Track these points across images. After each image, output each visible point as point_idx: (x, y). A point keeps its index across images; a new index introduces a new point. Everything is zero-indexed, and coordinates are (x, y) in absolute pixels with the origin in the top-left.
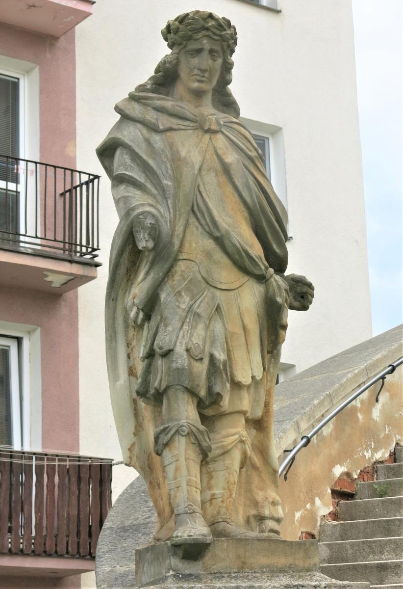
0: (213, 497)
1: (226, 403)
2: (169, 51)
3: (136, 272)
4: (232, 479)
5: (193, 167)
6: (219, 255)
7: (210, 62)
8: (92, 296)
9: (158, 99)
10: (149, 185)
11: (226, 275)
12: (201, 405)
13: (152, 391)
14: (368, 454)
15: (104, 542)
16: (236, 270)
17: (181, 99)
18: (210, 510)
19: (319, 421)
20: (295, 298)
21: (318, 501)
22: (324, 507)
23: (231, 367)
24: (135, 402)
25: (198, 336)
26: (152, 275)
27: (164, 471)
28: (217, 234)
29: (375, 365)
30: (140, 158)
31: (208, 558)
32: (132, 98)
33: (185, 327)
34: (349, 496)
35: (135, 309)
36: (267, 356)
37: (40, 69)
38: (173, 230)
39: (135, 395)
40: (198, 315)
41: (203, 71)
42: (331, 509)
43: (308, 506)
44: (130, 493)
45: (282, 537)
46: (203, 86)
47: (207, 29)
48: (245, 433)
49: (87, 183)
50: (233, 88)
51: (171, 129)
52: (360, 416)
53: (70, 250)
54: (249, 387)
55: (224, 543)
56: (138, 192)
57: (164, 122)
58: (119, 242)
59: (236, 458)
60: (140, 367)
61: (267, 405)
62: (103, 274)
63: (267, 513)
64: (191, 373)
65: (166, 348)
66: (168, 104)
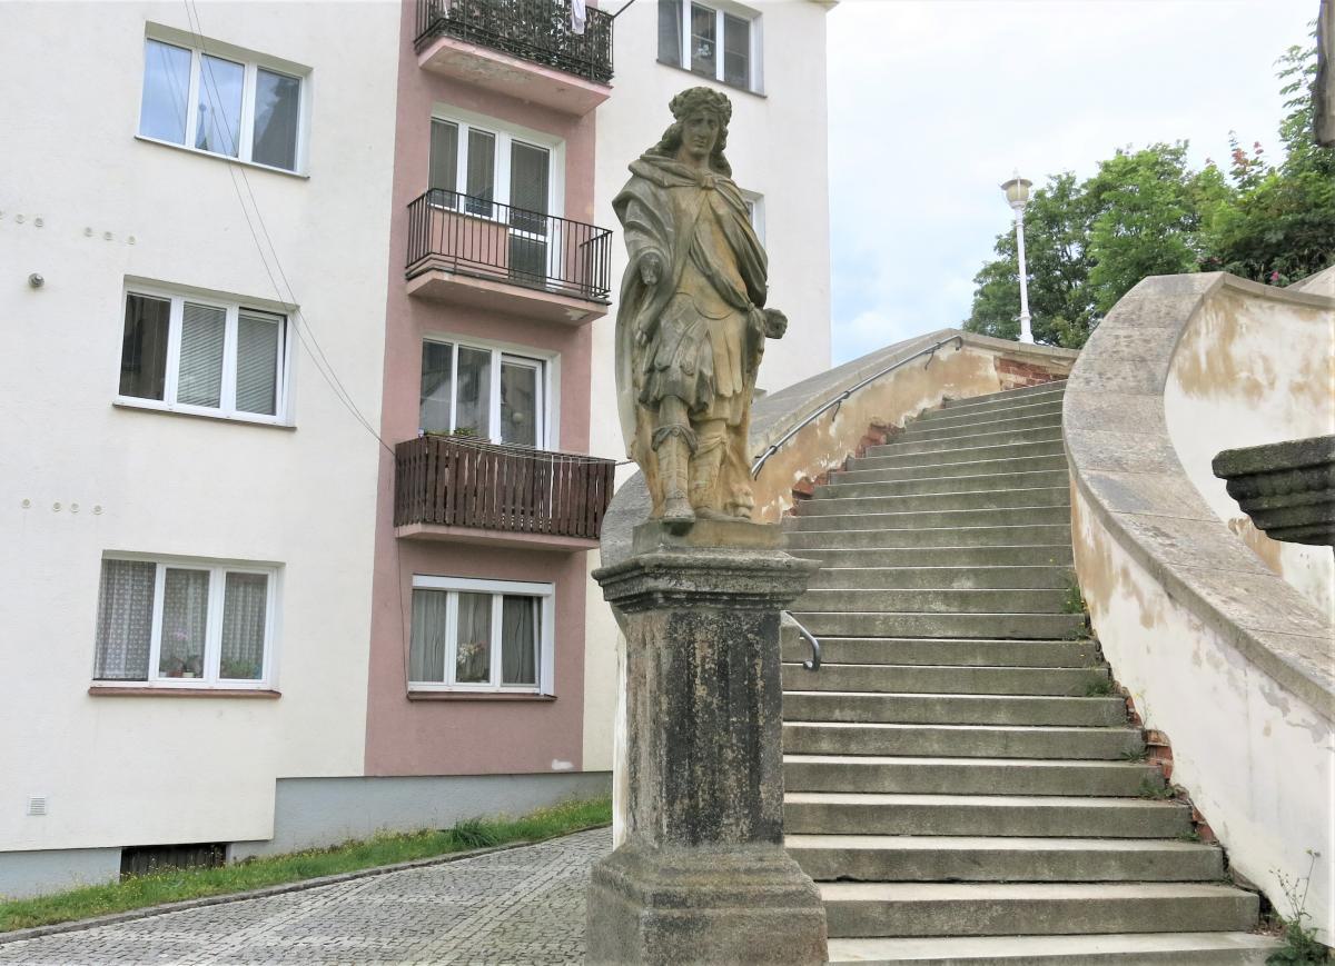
0: (697, 487)
1: (711, 412)
2: (675, 121)
3: (642, 304)
4: (713, 473)
5: (691, 218)
6: (710, 290)
7: (709, 130)
8: (604, 331)
9: (665, 161)
10: (654, 232)
11: (715, 307)
12: (690, 412)
13: (651, 399)
14: (824, 464)
15: (607, 523)
16: (724, 304)
17: (683, 161)
18: (695, 497)
19: (785, 434)
20: (771, 328)
21: (781, 499)
22: (785, 504)
23: (716, 380)
24: (637, 408)
25: (690, 356)
26: (654, 306)
27: (659, 464)
28: (709, 273)
29: (833, 390)
30: (647, 208)
31: (691, 535)
32: (643, 159)
33: (681, 348)
34: (807, 496)
35: (640, 333)
36: (746, 375)
37: (567, 145)
38: (673, 269)
39: (637, 402)
40: (691, 339)
41: (703, 138)
42: (792, 506)
43: (773, 503)
44: (630, 485)
45: (755, 520)
46: (702, 151)
47: (707, 102)
48: (725, 436)
49: (602, 237)
50: (726, 153)
51: (674, 186)
52: (819, 432)
53: (586, 291)
54: (730, 399)
55: (705, 524)
56: (645, 237)
57: (668, 179)
58: (628, 277)
59: (717, 456)
60: (642, 380)
61: (744, 414)
62: (613, 310)
63: (741, 501)
64: (683, 386)
65: (664, 365)
66: (673, 165)
